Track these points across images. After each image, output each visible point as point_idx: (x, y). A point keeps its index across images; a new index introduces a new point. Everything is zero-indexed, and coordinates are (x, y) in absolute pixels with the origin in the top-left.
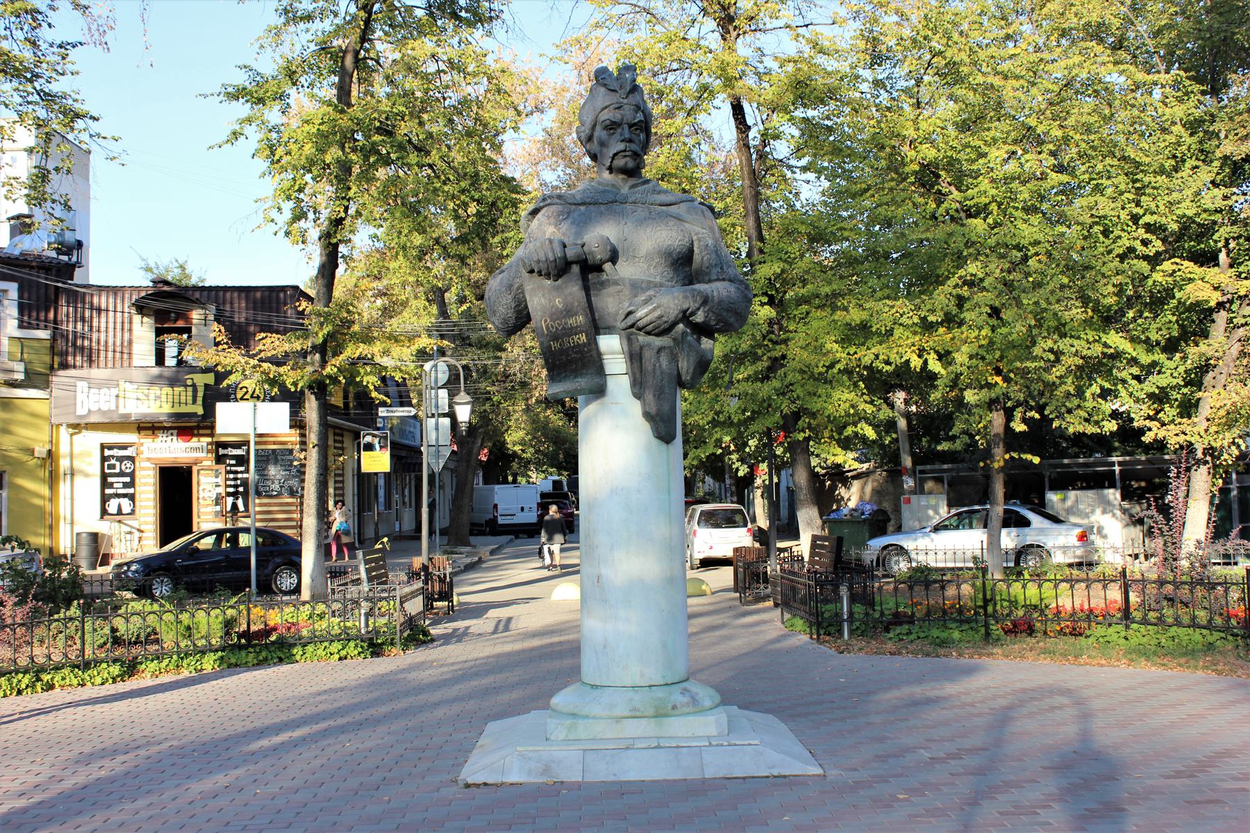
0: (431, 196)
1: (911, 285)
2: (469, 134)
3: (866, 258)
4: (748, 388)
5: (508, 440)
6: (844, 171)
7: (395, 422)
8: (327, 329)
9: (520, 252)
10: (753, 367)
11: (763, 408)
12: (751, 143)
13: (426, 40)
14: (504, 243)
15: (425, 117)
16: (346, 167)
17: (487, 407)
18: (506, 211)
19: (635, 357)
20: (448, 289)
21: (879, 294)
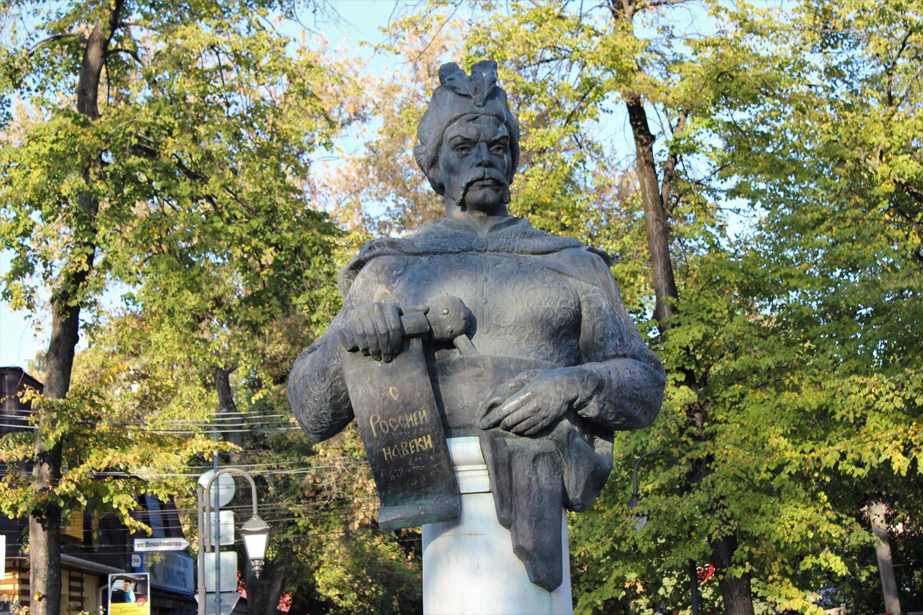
0: (208, 238)
1: (889, 352)
2: (263, 152)
3: (823, 315)
4: (661, 503)
5: (319, 581)
6: (787, 193)
7: (158, 559)
8: (62, 429)
9: (338, 322)
10: (668, 474)
11: (686, 531)
12: (657, 159)
13: (202, 24)
14: (313, 303)
15: (202, 130)
16: (89, 202)
17: (290, 535)
18: (316, 260)
19: (501, 467)
20: (233, 368)
21: (843, 367)
